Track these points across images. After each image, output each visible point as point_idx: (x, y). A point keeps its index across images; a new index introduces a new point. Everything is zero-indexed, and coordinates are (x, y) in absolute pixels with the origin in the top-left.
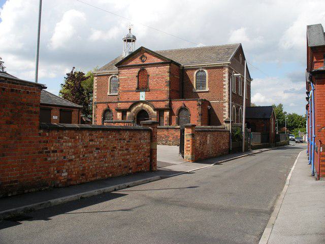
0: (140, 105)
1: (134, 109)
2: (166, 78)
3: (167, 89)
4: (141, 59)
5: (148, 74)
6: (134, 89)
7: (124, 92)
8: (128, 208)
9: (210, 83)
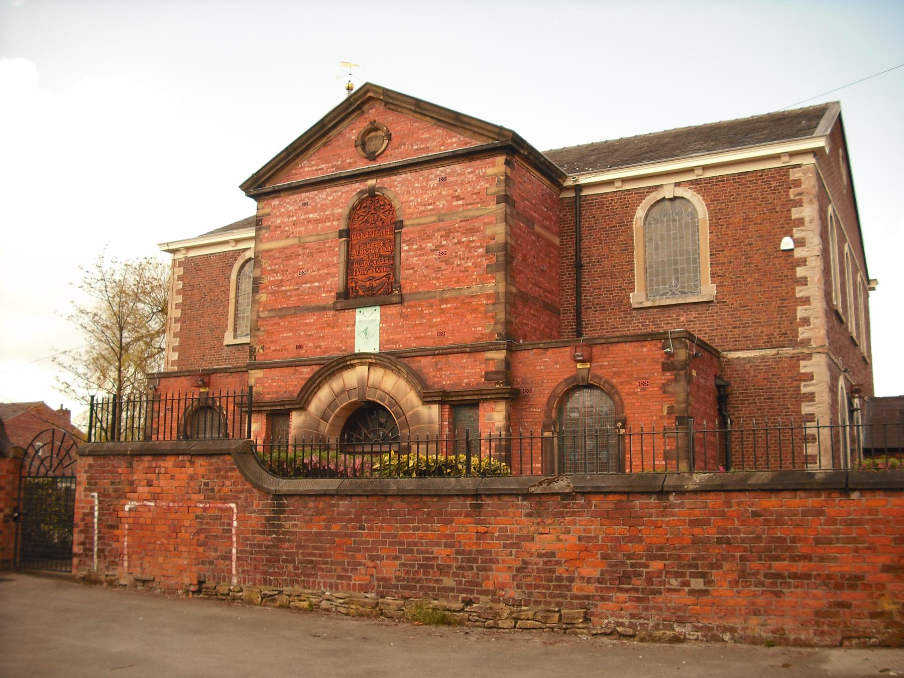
0: (352, 377)
1: (324, 394)
2: (489, 231)
3: (495, 285)
4: (363, 145)
5: (399, 215)
6: (327, 298)
7: (281, 314)
8: (660, 203)
9: (722, 258)
